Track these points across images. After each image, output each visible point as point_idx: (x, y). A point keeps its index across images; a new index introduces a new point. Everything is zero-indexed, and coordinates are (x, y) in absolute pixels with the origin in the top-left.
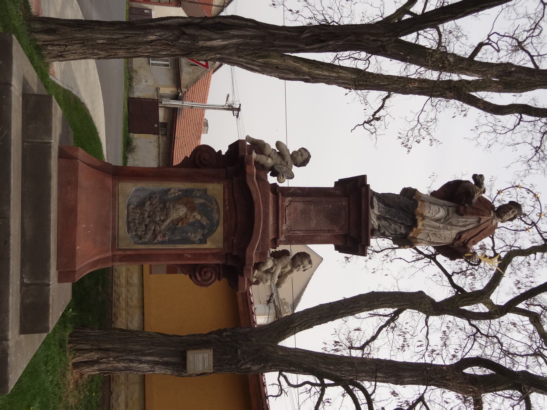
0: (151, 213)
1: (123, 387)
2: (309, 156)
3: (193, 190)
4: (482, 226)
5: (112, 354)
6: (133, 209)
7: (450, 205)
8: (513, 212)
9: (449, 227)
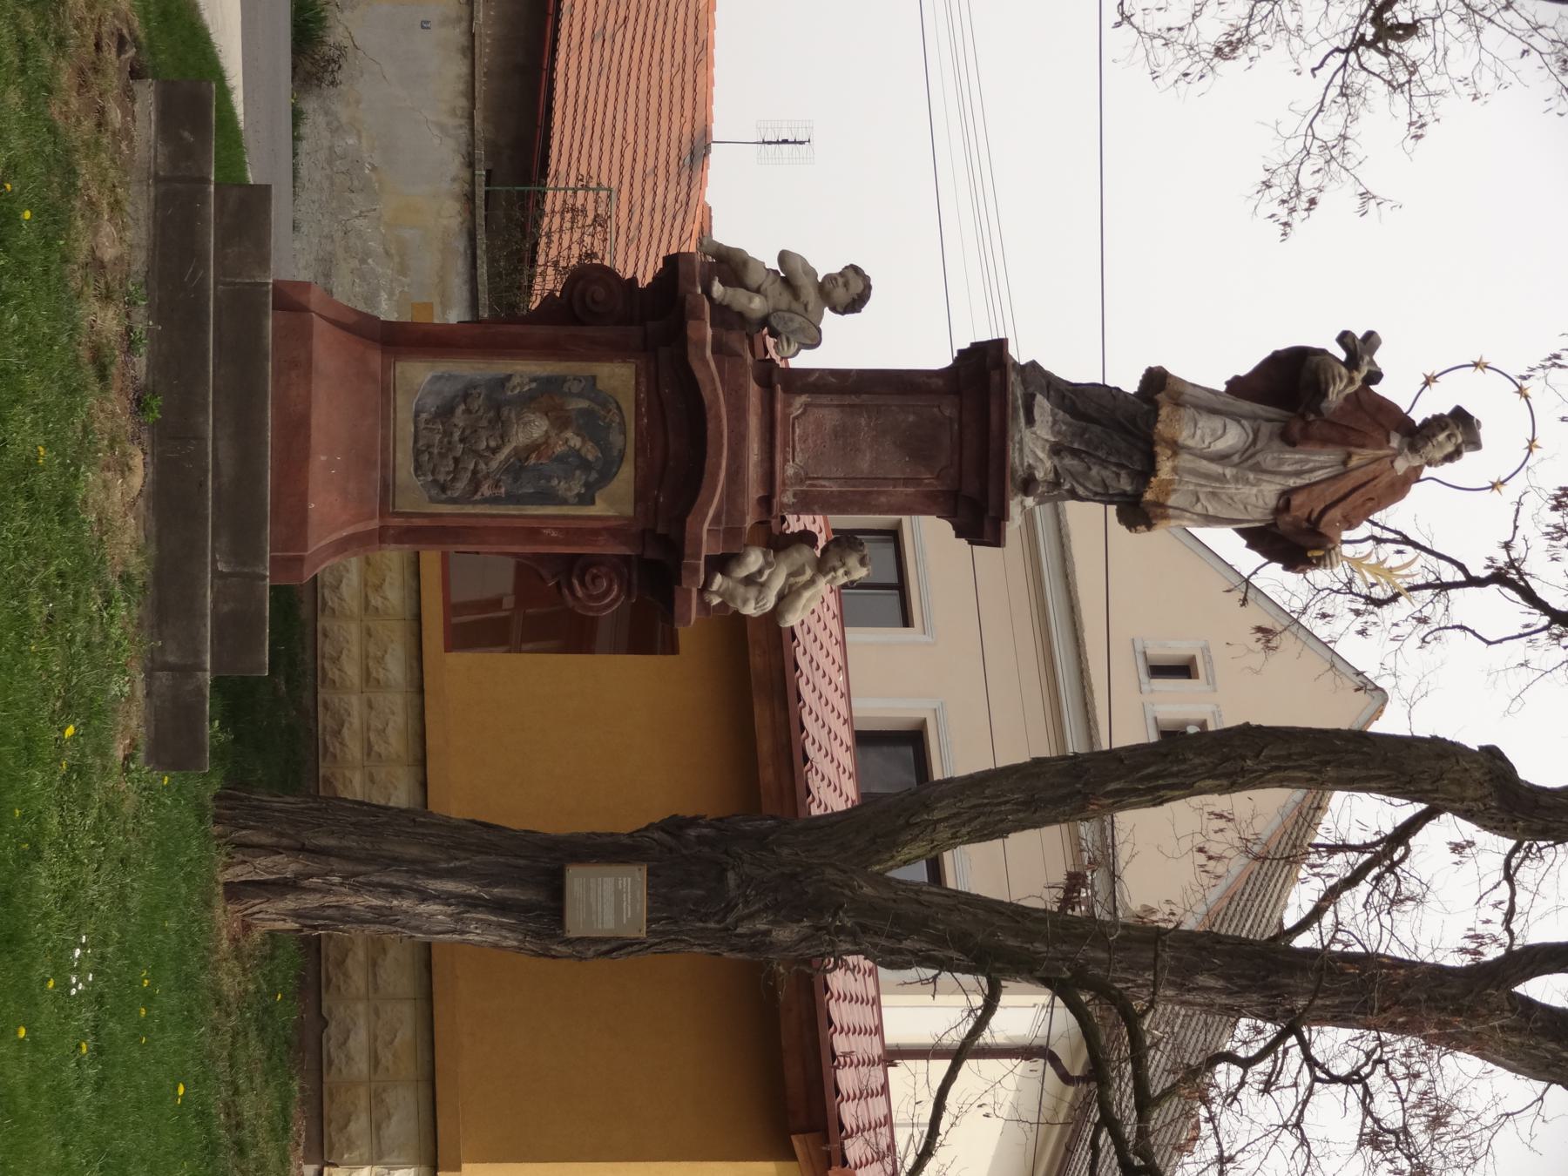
0: (468, 432)
1: (361, 1007)
2: (868, 287)
3: (564, 379)
4: (1356, 474)
5: (336, 864)
6: (427, 421)
7: (1273, 416)
8: (1449, 437)
9: (1251, 476)
